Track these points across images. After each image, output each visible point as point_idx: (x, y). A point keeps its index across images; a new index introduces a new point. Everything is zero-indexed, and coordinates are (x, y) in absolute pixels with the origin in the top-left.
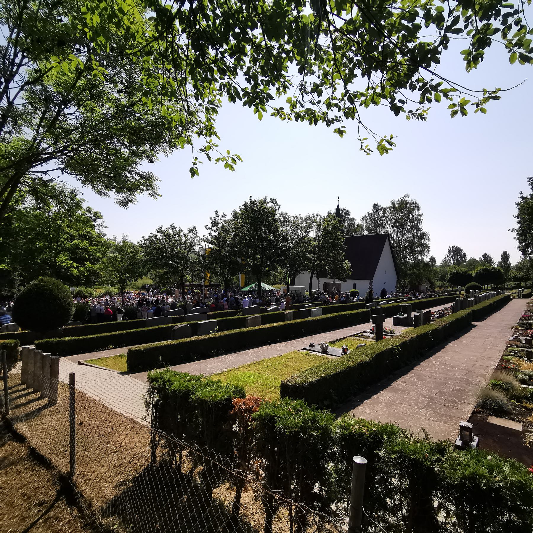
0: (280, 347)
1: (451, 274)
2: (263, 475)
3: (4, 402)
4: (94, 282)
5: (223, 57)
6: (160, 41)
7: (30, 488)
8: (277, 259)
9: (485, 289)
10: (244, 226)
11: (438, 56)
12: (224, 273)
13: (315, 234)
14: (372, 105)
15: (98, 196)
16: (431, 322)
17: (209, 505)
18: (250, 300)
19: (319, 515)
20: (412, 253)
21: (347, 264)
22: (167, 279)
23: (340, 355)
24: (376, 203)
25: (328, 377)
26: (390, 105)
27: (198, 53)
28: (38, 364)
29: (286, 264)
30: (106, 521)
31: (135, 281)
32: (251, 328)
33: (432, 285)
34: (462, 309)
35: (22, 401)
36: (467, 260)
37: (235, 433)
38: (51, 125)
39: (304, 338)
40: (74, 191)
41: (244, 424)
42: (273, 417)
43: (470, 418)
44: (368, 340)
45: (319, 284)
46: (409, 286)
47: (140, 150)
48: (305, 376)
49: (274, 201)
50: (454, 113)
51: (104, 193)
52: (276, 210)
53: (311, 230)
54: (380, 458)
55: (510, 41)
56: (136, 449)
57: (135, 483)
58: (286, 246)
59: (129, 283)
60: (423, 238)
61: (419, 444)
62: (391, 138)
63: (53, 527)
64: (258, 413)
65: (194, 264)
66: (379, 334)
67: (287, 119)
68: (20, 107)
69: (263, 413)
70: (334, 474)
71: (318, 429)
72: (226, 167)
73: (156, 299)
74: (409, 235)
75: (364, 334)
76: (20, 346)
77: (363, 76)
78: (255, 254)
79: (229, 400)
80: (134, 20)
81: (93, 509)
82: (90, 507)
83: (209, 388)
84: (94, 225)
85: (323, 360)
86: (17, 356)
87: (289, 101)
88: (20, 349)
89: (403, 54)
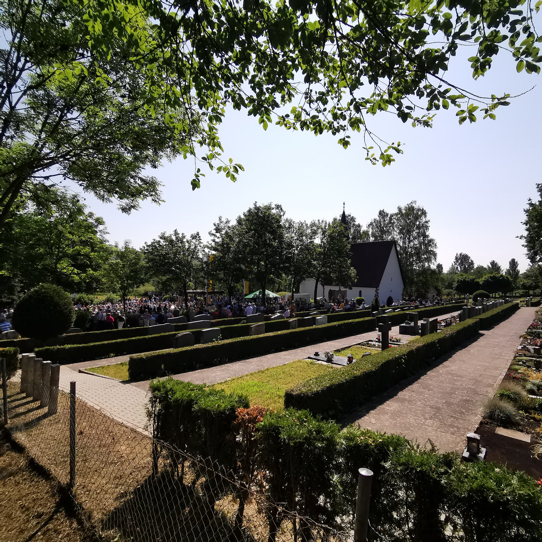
0: (285, 355)
1: (458, 281)
2: (267, 487)
3: (3, 410)
4: (95, 289)
7: (29, 500)
8: (282, 265)
9: (492, 297)
11: (446, 62)
13: (320, 241)
16: (438, 331)
17: (211, 518)
18: (254, 308)
19: (324, 528)
20: (419, 260)
21: (353, 271)
22: (169, 285)
23: (346, 364)
24: (382, 210)
28: (38, 373)
29: (290, 271)
30: (106, 534)
31: (137, 287)
33: (439, 293)
34: (469, 317)
35: (22, 410)
36: (475, 267)
37: (239, 444)
39: (309, 347)
40: (75, 196)
41: (247, 435)
42: (277, 428)
45: (324, 291)
46: (416, 294)
47: (143, 155)
49: (278, 207)
50: (463, 120)
51: (106, 199)
52: (281, 216)
53: (316, 237)
54: (385, 470)
55: (518, 49)
57: (136, 494)
58: (290, 253)
59: (131, 290)
60: (430, 245)
61: (426, 456)
62: (399, 145)
63: (52, 540)
64: (262, 423)
65: (197, 271)
66: (385, 343)
68: (22, 111)
69: (267, 423)
70: (339, 486)
71: (323, 440)
73: (158, 306)
74: (416, 242)
75: (370, 342)
76: (20, 354)
77: (370, 83)
78: (259, 260)
79: (233, 409)
81: (93, 521)
82: (90, 519)
83: (212, 398)
84: (96, 232)
85: (328, 369)
86: (17, 364)
88: (20, 356)
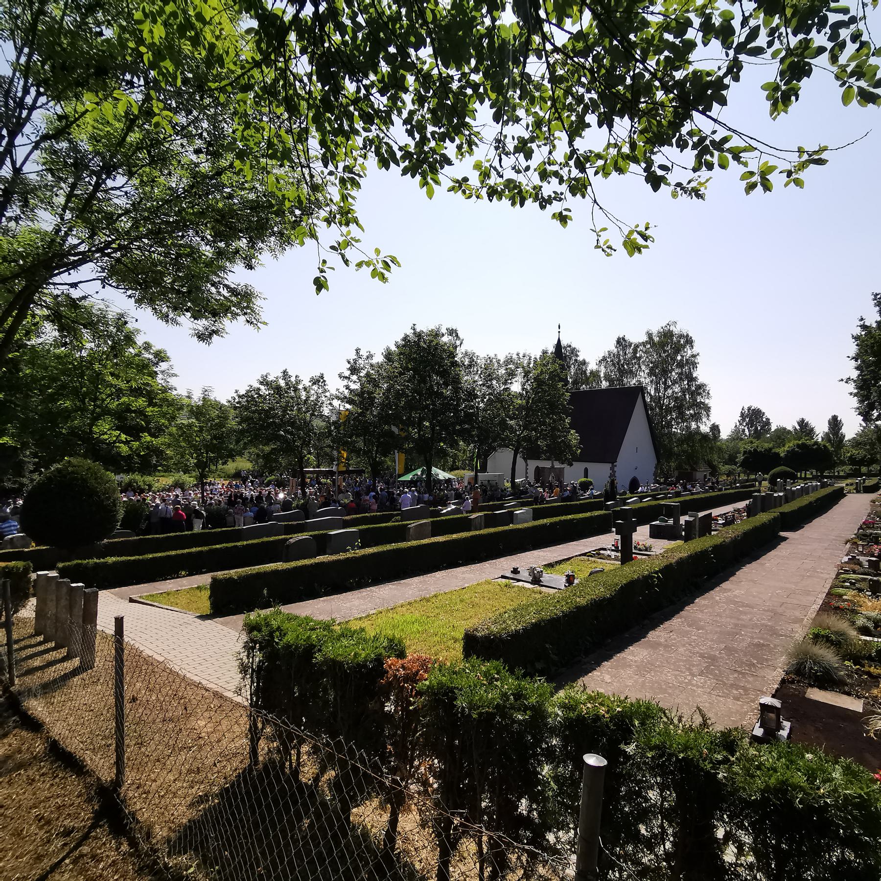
0: (463, 573)
1: (745, 452)
2: (435, 786)
3: (7, 664)
4: (156, 466)
5: (368, 94)
6: (264, 67)
7: (50, 807)
8: (458, 427)
9: (801, 478)
10: (404, 374)
11: (724, 92)
12: (370, 451)
13: (520, 387)
14: (614, 174)
15: (162, 323)
16: (713, 533)
17: (345, 835)
18: (413, 496)
19: (527, 851)
20: (682, 419)
21: (574, 437)
22: (276, 460)
23: (563, 587)
24: (621, 336)
25: (543, 624)
26: (645, 174)
27: (327, 88)
28: (64, 602)
29: (472, 436)
30: (175, 862)
31: (223, 464)
32: (414, 543)
33: (714, 471)
34: (763, 510)
35: (37, 662)
36: (773, 430)
37: (389, 715)
38: (85, 206)
39: (502, 559)
40: (121, 316)
41: (402, 701)
42: (451, 690)
43: (776, 691)
44: (608, 562)
45: (527, 469)
46: (676, 473)
47: (232, 249)
48: (504, 622)
49: (452, 332)
50: (751, 187)
51: (172, 319)
52: (456, 347)
53: (513, 380)
54: (627, 757)
55: (843, 68)
56: (224, 742)
57: (223, 798)
58: (472, 407)
59: (213, 468)
60: (700, 394)
61: (692, 735)
62: (647, 229)
63: (87, 871)
64: (427, 683)
65: (321, 436)
66: (626, 552)
67: (474, 197)
68: (33, 177)
69: (435, 682)
70: (552, 783)
71: (526, 709)
72: (373, 277)
73: (257, 494)
74: (677, 388)
75: (602, 552)
76: (33, 572)
77: (600, 125)
78: (422, 420)
79: (379, 660)
80: (221, 33)
81: (154, 841)
82: (148, 837)
83: (345, 642)
84: (156, 373)
85: (533, 595)
86: (29, 589)
87: (478, 166)
88: (33, 576)
89: (667, 90)
